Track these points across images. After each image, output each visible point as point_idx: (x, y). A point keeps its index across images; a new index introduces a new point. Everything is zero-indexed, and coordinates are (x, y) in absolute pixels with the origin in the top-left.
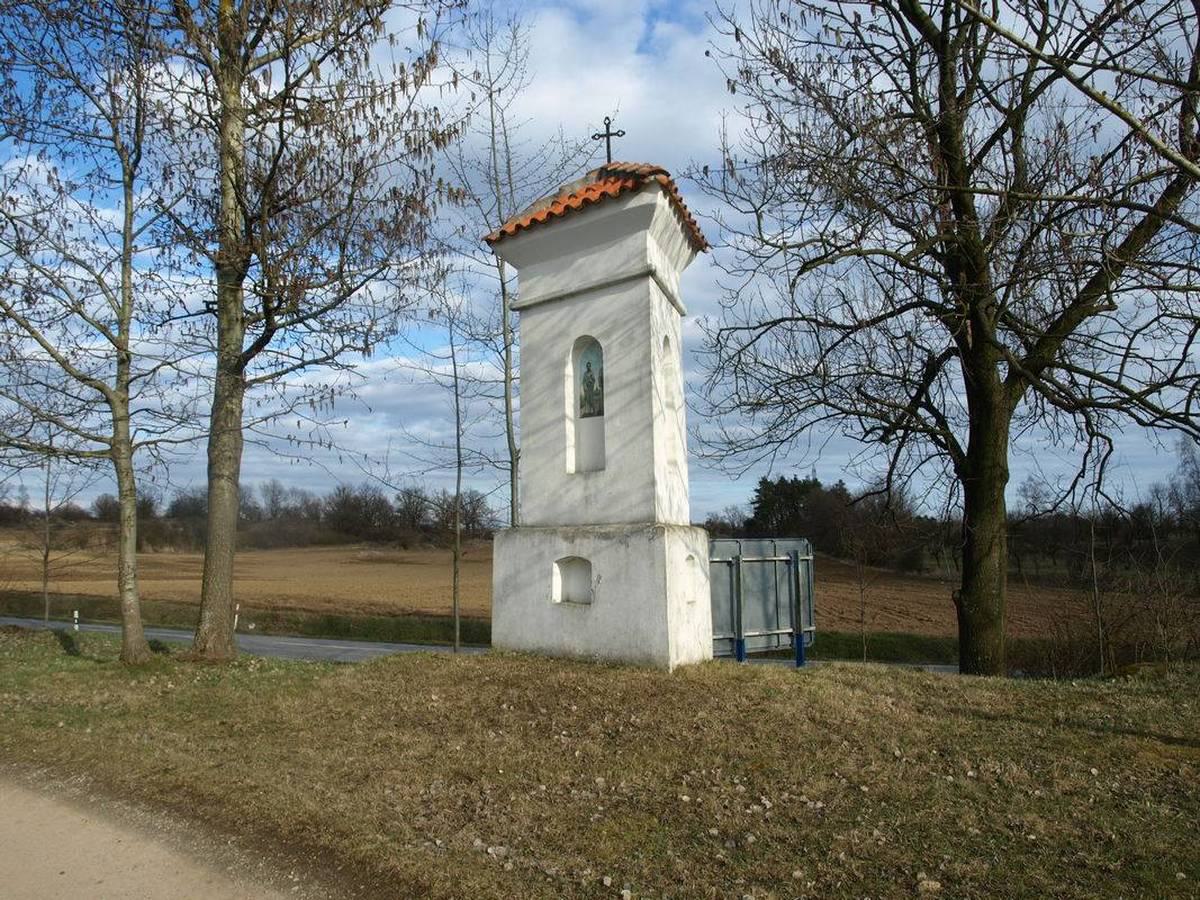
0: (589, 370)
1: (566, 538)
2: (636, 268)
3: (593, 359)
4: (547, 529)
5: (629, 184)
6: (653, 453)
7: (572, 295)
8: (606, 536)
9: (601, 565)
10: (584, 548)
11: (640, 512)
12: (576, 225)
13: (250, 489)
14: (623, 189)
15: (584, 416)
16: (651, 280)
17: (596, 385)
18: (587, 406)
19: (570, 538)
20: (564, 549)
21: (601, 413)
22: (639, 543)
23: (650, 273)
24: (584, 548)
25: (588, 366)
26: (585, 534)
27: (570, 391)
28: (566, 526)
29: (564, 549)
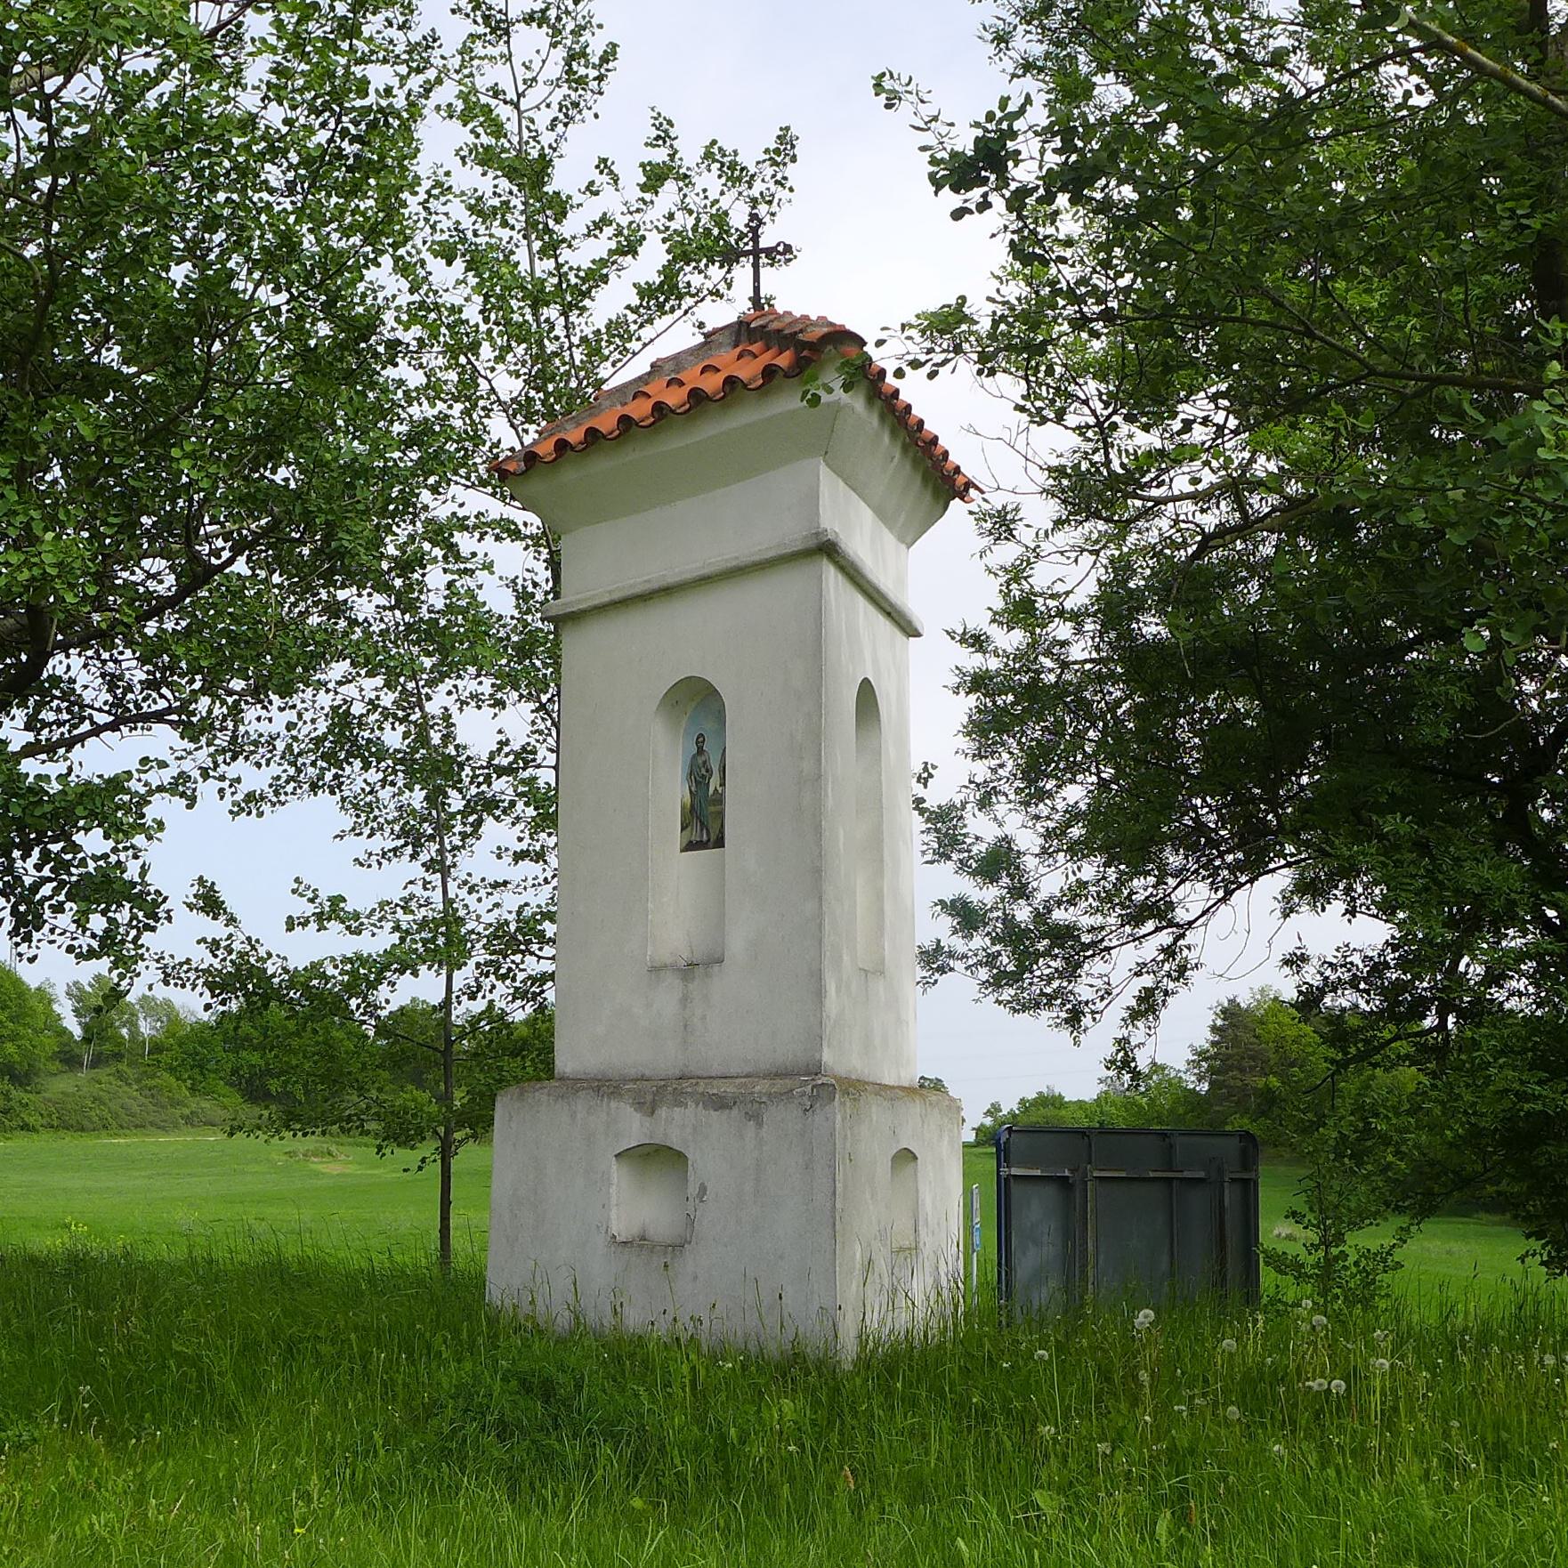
0: (700, 751)
1: (639, 1105)
2: (793, 535)
3: (708, 727)
4: (604, 1086)
5: (784, 360)
6: (820, 926)
7: (667, 592)
8: (720, 1103)
9: (706, 1162)
10: (674, 1125)
11: (785, 1048)
12: (690, 440)
13: (44, 996)
14: (769, 372)
15: (690, 846)
16: (831, 574)
17: (714, 782)
18: (696, 825)
19: (648, 1107)
20: (634, 1128)
21: (720, 843)
22: (782, 1117)
23: (828, 549)
24: (674, 1125)
25: (700, 741)
26: (679, 1099)
27: (674, 792)
28: (747, 1076)
29: (634, 1128)
